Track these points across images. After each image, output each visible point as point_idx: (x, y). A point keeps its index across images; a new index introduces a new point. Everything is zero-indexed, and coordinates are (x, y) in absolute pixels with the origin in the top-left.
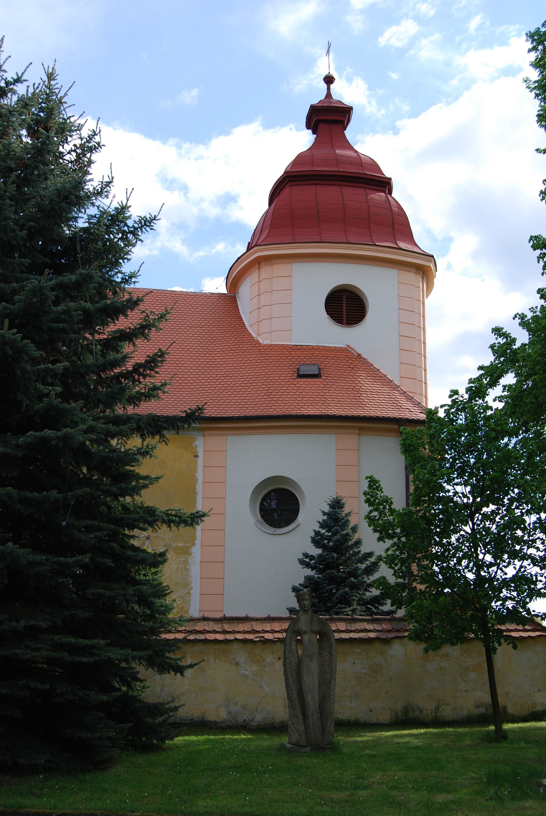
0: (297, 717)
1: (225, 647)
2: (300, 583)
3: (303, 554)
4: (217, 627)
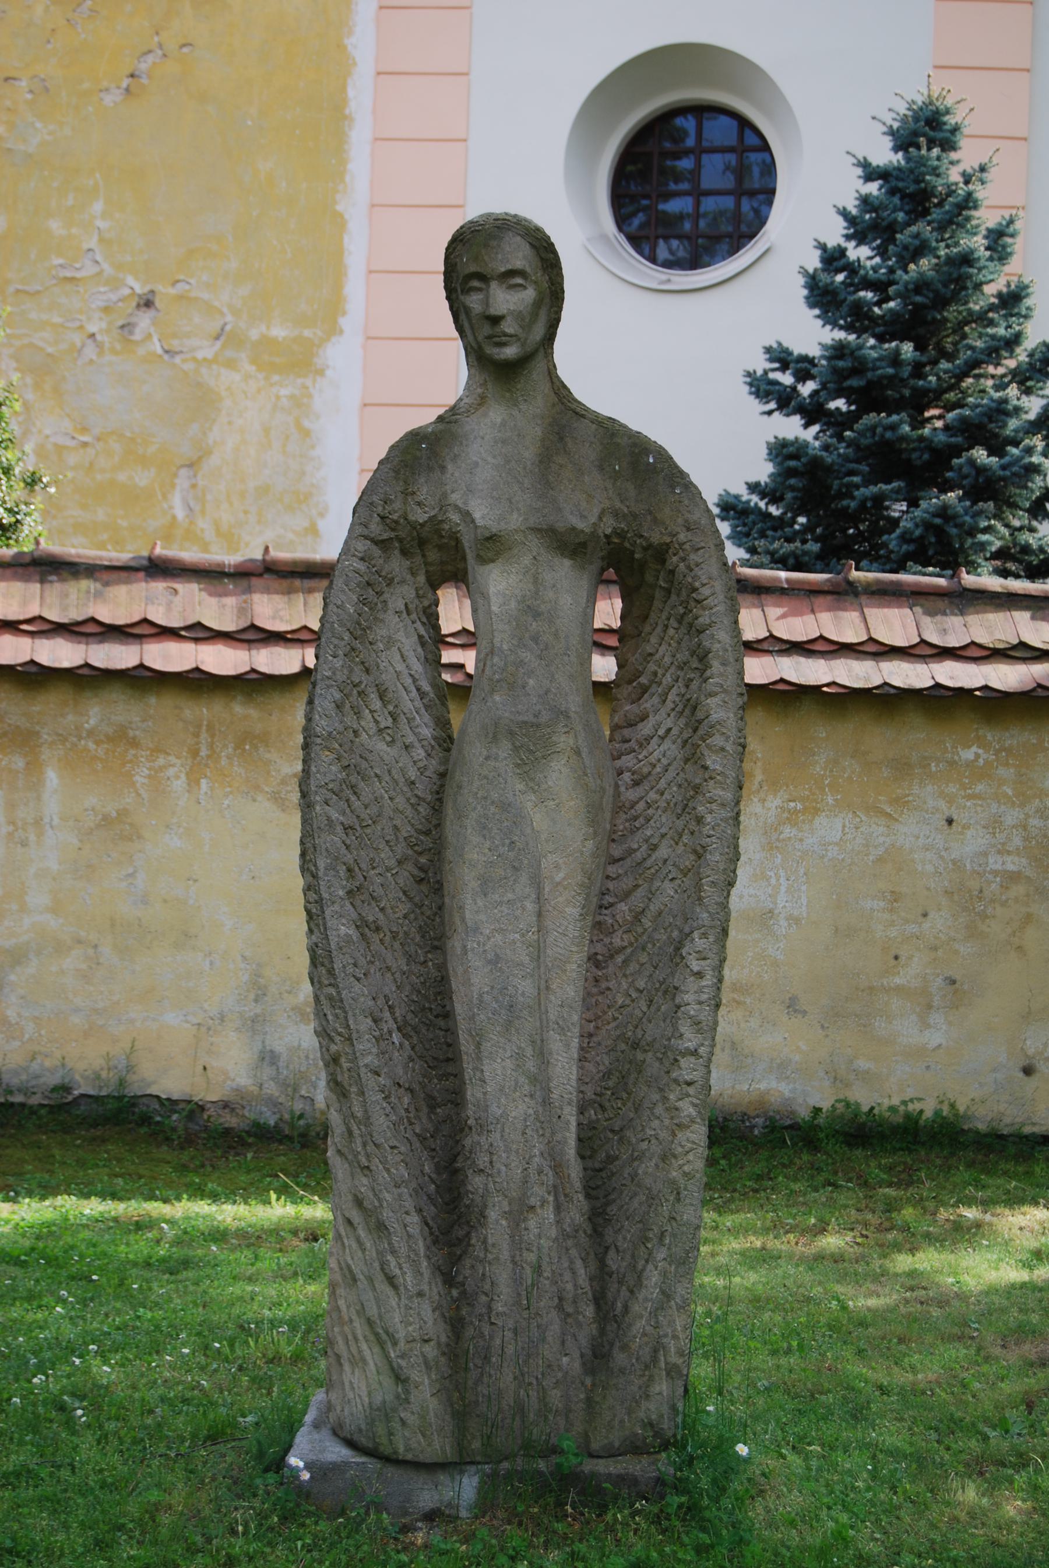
0: (381, 1228)
1: (253, 712)
2: (752, 479)
3: (768, 350)
4: (218, 611)
